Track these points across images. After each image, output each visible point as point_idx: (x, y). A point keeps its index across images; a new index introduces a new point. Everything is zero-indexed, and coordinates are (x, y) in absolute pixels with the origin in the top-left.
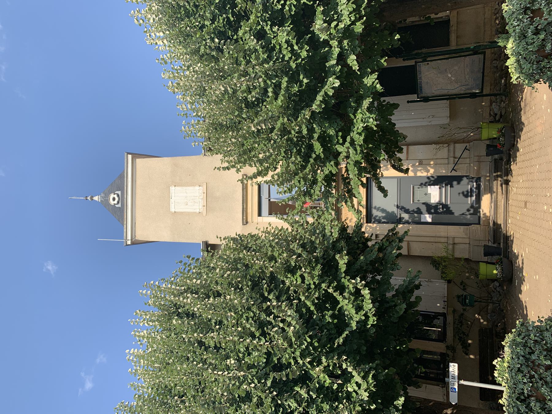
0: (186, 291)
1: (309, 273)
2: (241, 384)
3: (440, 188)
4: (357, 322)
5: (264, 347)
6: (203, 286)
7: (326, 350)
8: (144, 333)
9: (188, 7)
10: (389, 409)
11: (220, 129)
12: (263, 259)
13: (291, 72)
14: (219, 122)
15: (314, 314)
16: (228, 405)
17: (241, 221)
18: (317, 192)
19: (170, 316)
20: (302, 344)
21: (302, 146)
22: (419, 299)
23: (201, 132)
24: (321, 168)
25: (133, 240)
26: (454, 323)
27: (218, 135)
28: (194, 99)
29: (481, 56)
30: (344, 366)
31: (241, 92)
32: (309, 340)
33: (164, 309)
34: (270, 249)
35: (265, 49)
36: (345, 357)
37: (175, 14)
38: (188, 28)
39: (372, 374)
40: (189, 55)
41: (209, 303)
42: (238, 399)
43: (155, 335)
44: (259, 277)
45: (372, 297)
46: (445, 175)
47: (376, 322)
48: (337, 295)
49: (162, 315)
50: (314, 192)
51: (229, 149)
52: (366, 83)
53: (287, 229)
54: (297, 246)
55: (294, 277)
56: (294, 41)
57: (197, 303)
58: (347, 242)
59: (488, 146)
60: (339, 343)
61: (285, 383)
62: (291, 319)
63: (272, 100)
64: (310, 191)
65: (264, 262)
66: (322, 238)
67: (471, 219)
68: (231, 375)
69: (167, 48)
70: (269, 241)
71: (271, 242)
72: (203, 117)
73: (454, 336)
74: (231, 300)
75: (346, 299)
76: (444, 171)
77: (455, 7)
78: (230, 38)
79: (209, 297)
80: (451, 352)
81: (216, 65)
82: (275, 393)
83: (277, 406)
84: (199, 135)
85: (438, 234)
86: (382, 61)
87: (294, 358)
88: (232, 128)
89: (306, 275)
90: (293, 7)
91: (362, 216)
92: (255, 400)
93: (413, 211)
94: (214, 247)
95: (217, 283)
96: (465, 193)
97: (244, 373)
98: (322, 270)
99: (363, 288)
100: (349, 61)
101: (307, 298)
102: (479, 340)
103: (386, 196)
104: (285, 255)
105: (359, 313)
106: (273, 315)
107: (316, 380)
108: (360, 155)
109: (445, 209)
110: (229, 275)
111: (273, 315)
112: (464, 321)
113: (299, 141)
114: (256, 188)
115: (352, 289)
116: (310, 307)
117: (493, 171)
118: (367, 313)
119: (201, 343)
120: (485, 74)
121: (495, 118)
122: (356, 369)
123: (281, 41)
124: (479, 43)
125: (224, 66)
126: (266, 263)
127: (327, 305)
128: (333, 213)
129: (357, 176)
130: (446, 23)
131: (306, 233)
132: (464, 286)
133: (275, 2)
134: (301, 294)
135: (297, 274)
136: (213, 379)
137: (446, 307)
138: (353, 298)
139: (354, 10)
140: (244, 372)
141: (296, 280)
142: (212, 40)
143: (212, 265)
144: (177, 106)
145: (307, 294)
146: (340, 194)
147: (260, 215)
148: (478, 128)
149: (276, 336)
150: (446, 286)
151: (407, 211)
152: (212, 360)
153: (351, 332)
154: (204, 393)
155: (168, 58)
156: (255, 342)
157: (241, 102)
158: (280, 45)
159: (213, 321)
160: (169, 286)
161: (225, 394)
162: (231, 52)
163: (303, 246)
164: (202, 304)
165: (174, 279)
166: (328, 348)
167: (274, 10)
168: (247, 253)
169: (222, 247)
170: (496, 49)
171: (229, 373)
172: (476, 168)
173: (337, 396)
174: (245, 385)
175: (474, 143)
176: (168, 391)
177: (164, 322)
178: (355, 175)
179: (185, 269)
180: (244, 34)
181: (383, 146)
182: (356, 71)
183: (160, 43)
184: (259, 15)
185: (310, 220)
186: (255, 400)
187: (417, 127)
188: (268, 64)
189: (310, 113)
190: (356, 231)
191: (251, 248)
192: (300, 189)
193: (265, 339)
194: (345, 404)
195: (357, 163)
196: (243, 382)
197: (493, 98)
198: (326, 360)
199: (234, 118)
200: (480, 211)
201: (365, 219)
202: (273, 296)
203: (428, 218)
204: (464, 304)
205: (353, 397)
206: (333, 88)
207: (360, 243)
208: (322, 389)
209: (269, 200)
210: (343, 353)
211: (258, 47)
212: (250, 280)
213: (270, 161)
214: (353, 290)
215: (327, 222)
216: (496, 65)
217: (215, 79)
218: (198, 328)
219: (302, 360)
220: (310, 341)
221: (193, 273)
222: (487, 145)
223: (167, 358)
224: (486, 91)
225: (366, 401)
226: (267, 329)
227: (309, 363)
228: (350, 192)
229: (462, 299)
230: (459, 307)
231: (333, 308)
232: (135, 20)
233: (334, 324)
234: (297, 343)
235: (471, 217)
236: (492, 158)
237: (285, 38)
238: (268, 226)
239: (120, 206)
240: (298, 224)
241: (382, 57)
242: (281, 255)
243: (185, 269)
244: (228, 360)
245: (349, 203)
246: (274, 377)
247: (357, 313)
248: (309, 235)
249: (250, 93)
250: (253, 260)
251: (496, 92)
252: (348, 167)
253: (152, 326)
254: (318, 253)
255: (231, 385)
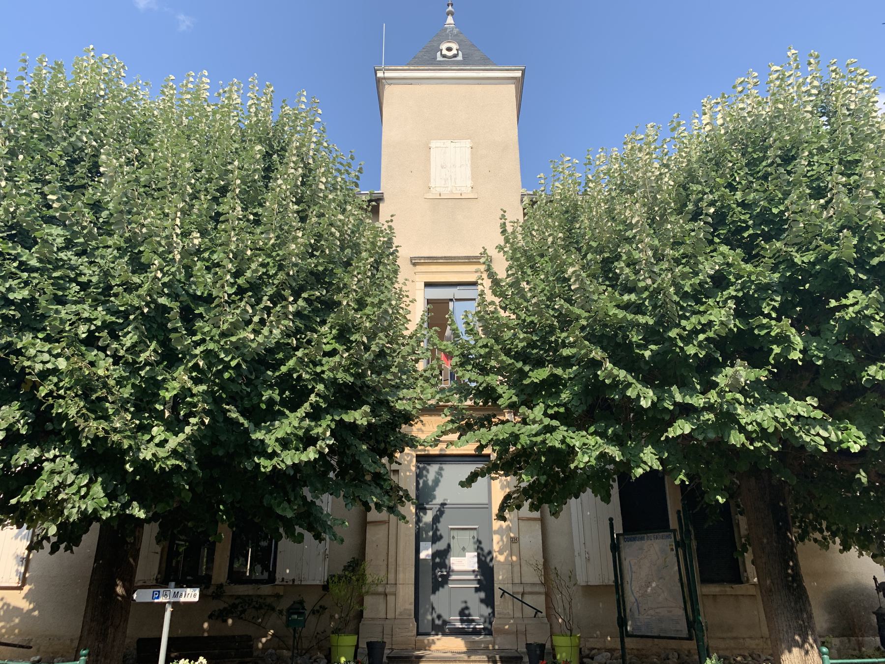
0: (306, 166)
1: (340, 364)
2: (160, 255)
3: (474, 571)
4: (262, 441)
5: (220, 292)
6: (314, 193)
7: (218, 391)
8: (236, 99)
9: (764, 164)
10: (125, 492)
11: (567, 219)
12: (359, 290)
13: (661, 330)
14: (579, 216)
15: (274, 372)
16: (127, 235)
17: (417, 256)
18: (468, 375)
19: (265, 140)
20: (227, 352)
21: (542, 349)
22: (300, 539)
23: (561, 187)
24: (505, 382)
25: (384, 81)
26: (259, 596)
27: (557, 216)
28: (616, 175)
29: (685, 633)
30: (193, 420)
31: (629, 250)
32: (233, 363)
33: (276, 130)
34: (376, 301)
35: (699, 288)
36: (207, 421)
37: (752, 142)
38: (731, 164)
39: (181, 464)
40: (687, 165)
41: (288, 203)
42: (136, 251)
43: (233, 116)
44: (330, 284)
45: (303, 464)
46: (495, 579)
47: (263, 470)
48: (306, 409)
49: (267, 127)
50: (468, 371)
51: (534, 233)
52: (645, 452)
53: (407, 329)
54: (383, 344)
55: (332, 339)
56: (711, 334)
57: (289, 184)
58: (387, 423)
59: (542, 646)
60: (230, 411)
61: (163, 327)
62: (267, 334)
63: (616, 300)
64: (470, 364)
65: (355, 290)
66: (393, 383)
67: (426, 621)
68: (175, 239)
69: (695, 132)
70: (389, 300)
71: (388, 303)
72: (586, 190)
73: (238, 597)
74: (297, 238)
75: (299, 423)
76: (501, 577)
77: (763, 591)
78: (714, 232)
79: (297, 203)
80: (213, 592)
81: (671, 210)
82: (146, 310)
83: (125, 315)
84: (557, 184)
85: (400, 569)
86: (681, 477)
87: (203, 341)
88: (568, 237)
89: (337, 358)
90: (765, 331)
91: (429, 448)
92: (136, 279)
93: (437, 529)
94: (375, 211)
95: (321, 215)
96: (467, 612)
97: (177, 260)
98: (345, 384)
99: (317, 450)
100: (680, 422)
101: (300, 360)
102: (234, 637)
103: (462, 484)
104: (368, 324)
105: (277, 444)
106: (272, 305)
107: (168, 376)
108: (528, 442)
109: (440, 579)
110: (332, 234)
111: (272, 305)
112: (263, 611)
113: (550, 346)
114: (472, 278)
115: (315, 431)
116: (285, 365)
117: (503, 654)
118: (278, 455)
119: (223, 190)
120: (656, 640)
121: (587, 656)
122: (187, 439)
123: (711, 314)
124: (707, 630)
125: (671, 223)
126: (354, 294)
127: (287, 393)
128: (433, 402)
129: (495, 438)
130: (736, 577)
131: (403, 357)
132: (318, 611)
133: (773, 303)
134: (306, 351)
135: (337, 345)
136: (167, 211)
137: (285, 583)
138: (301, 433)
139: (764, 430)
140: (180, 261)
141: (328, 343)
142: (712, 204)
143: (349, 208)
144: (602, 149)
145: (306, 360)
146: (464, 411)
147: (428, 285)
148: (571, 631)
149: (238, 311)
150: (318, 583)
151: (436, 519)
152: (198, 209)
153: (246, 432)
154: (145, 196)
155: (681, 133)
156: (228, 277)
157: (611, 251)
158: (705, 312)
159: (260, 210)
160: (314, 139)
161: (144, 230)
162: (693, 234)
163: (381, 354)
164: (286, 192)
165: (325, 147)
166: (220, 395)
167: (760, 301)
168: (369, 264)
169: (377, 224)
170: (697, 657)
171: (177, 235)
172: (507, 627)
173: (145, 411)
174: (159, 262)
175: (546, 624)
176: (144, 137)
177: (256, 131)
178: (496, 435)
179: (341, 164)
180: (722, 254)
181: (543, 478)
182: (666, 434)
183: (706, 119)
184: (753, 278)
185: (421, 366)
186: (136, 279)
187: (571, 534)
188: (675, 294)
189: (599, 358)
190: (405, 438)
191: (377, 270)
192: (472, 348)
193: (233, 294)
194: (133, 423)
195: (515, 437)
196: (164, 259)
197: (618, 654)
198: (201, 391)
199: (586, 240)
200: (437, 635)
201: (423, 453)
202: (301, 306)
203: (426, 553)
204: (291, 611)
205: (143, 435)
206: (639, 396)
207: (386, 445)
208: (155, 385)
209: (451, 300)
210: (213, 419)
211: (701, 277)
212: (325, 270)
213: (517, 299)
214: (314, 432)
215: (419, 391)
216: (670, 657)
217: (650, 209)
218: (248, 187)
219: (201, 352)
220: (233, 366)
221: (335, 177)
222: (544, 645)
223: (198, 136)
224: (630, 643)
225: (138, 457)
226: (249, 296)
227: (197, 364)
228: (469, 427)
229: (298, 608)
230: (285, 604)
231: (283, 403)
232: (742, 79)
233: (259, 403)
234: (227, 345)
235: (428, 620)
236: (523, 653)
237: (716, 320)
238: (411, 299)
239: (438, 59)
240: (415, 345)
241: (686, 475)
242: (367, 318)
243: (341, 164)
244: (198, 235)
245: (450, 426)
246: (172, 309)
247: (277, 440)
248: (399, 363)
249: (628, 265)
250: (358, 274)
251: (628, 657)
252: (509, 424)
253: (249, 111)
254: (371, 378)
255: (158, 239)
